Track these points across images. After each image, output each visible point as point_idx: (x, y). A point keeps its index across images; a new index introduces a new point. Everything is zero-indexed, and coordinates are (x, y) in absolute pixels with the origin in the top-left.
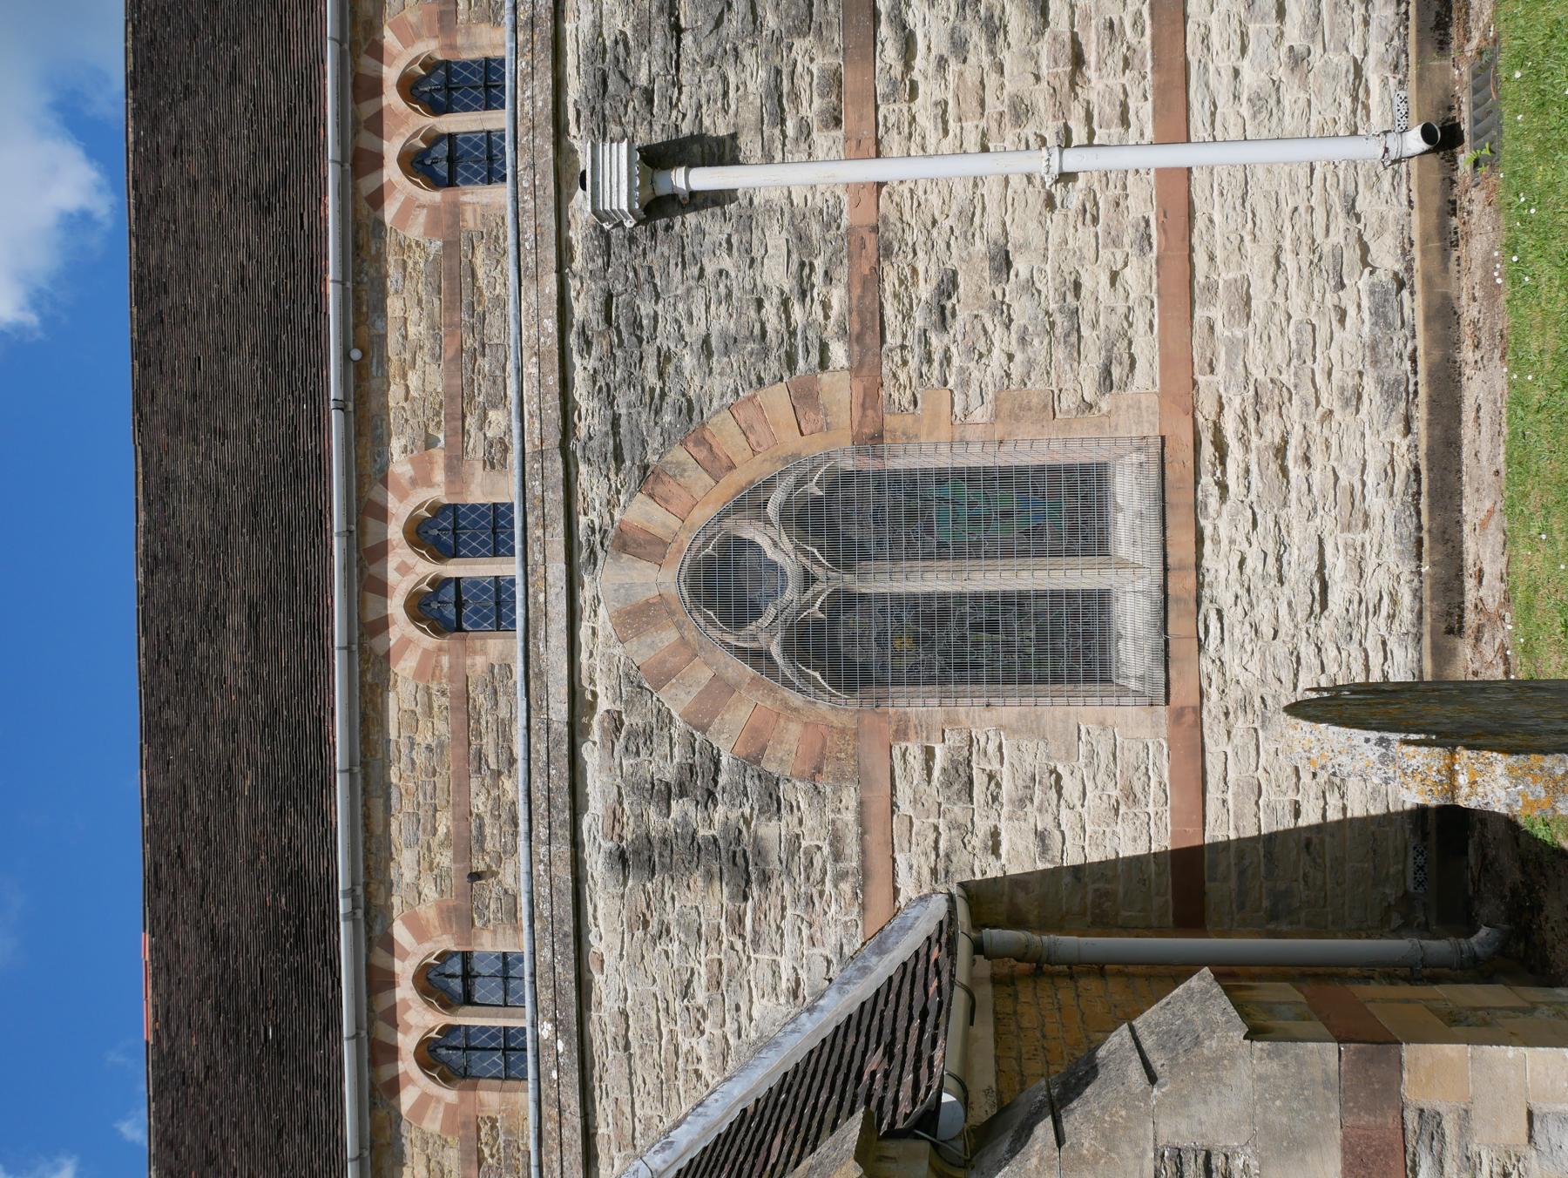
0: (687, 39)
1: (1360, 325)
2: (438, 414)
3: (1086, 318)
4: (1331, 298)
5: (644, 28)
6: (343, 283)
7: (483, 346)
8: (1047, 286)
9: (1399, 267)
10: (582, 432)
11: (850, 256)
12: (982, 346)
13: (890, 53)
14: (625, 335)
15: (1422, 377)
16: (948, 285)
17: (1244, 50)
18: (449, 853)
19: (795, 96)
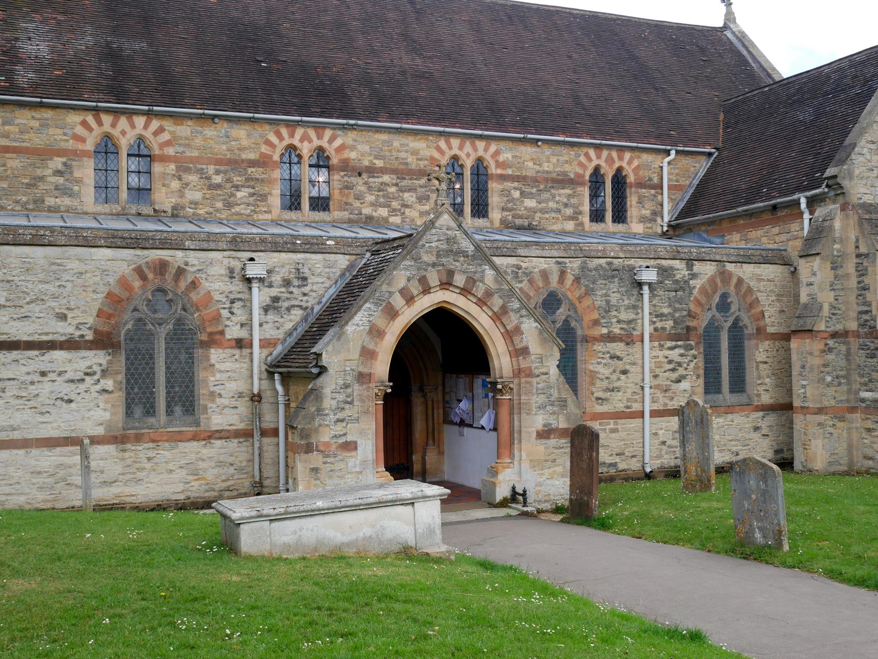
0: (674, 294)
3: (612, 393)
7: (541, 191)
13: (669, 344)
19: (661, 320)
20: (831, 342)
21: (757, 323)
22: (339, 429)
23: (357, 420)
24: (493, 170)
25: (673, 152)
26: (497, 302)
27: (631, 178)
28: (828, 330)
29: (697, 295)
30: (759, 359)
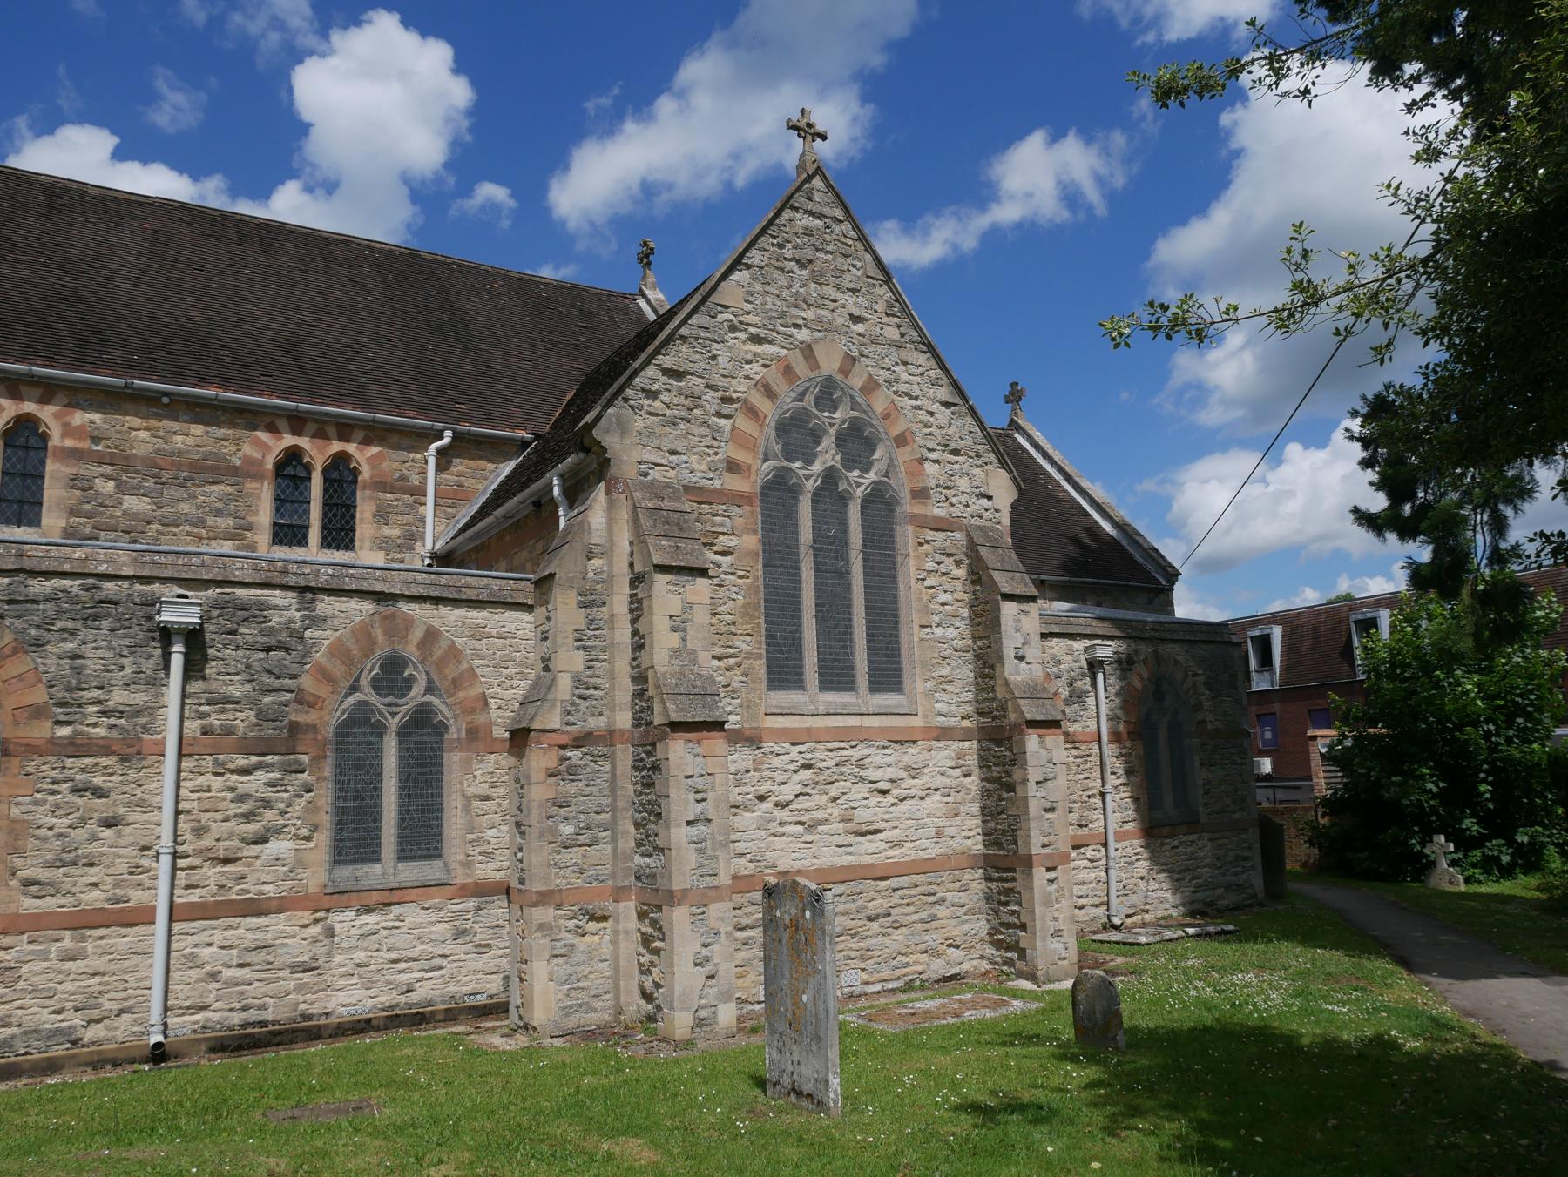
0: (262, 655)
1: (49, 1021)
2: (116, 448)
3: (72, 870)
4: (69, 1005)
5: (272, 632)
6: (216, 399)
8: (93, 848)
9: (86, 1040)
10: (30, 582)
11: (124, 739)
12: (59, 812)
13: (241, 762)
14: (90, 611)
15: (13, 1059)
16: (100, 793)
17: (223, 948)
19: (222, 711)
21: (469, 719)
25: (448, 433)
29: (323, 661)
30: (470, 791)
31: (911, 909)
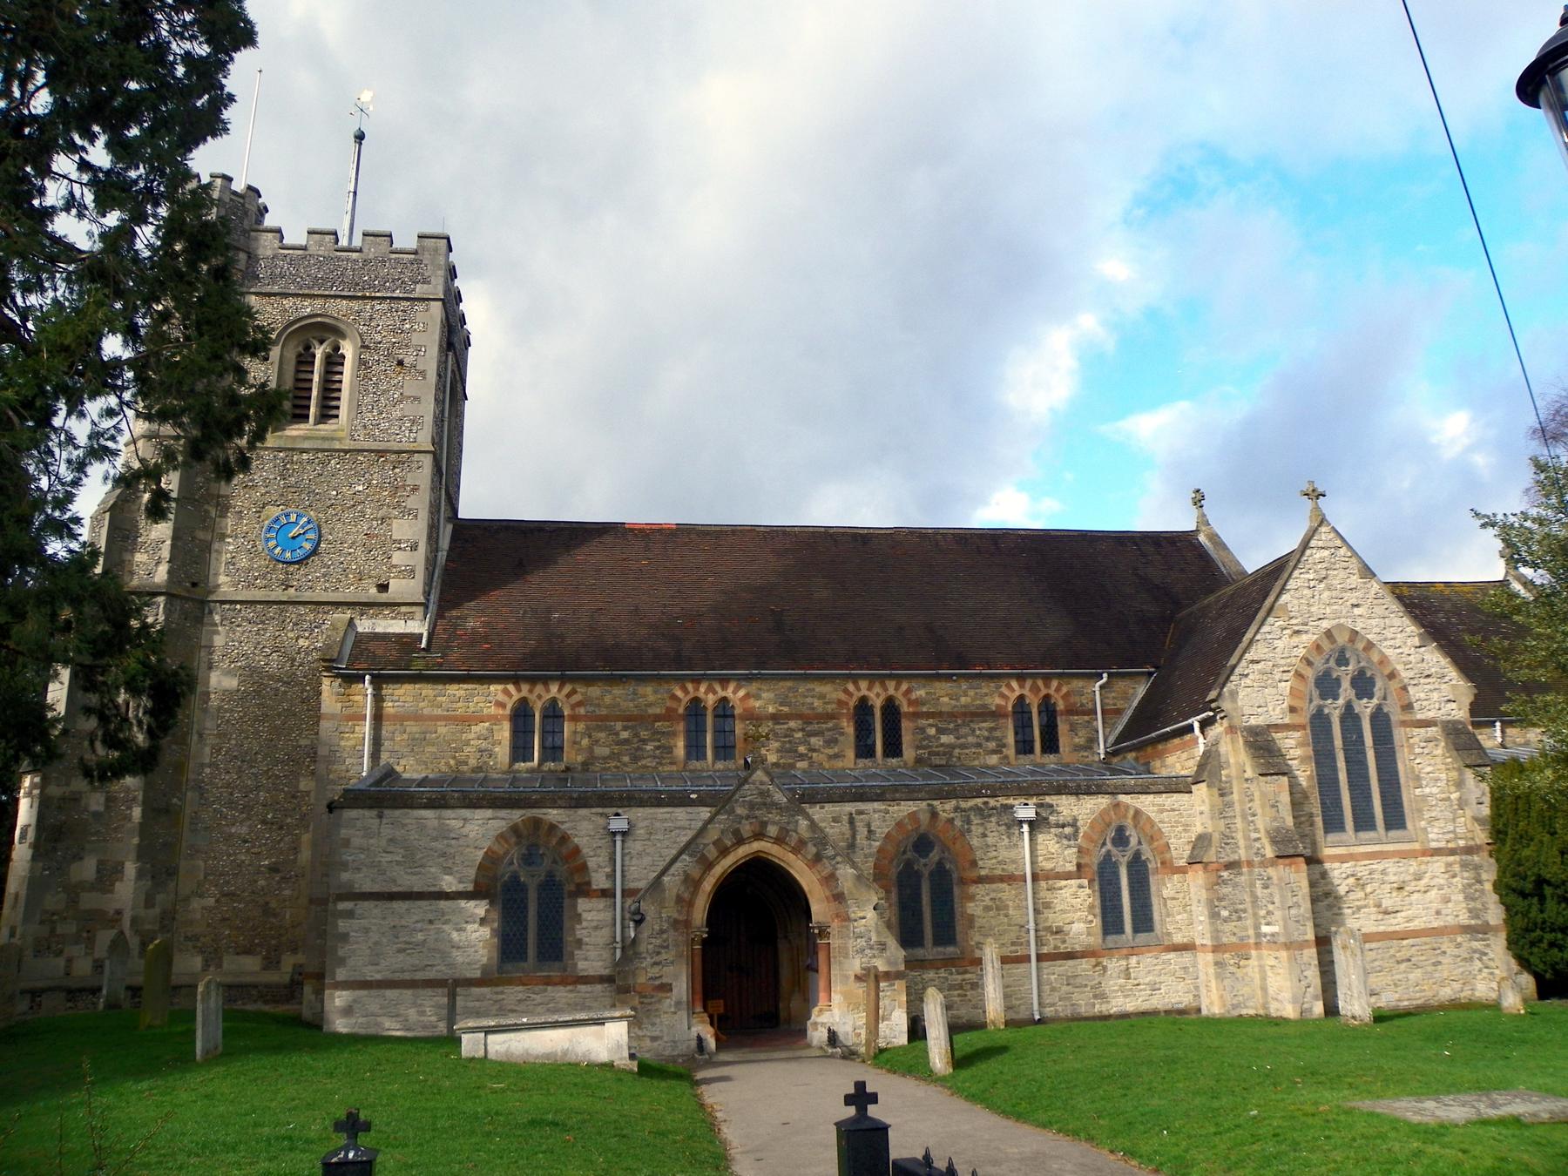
18: (774, 711)
20: (1225, 874)
22: (654, 971)
23: (672, 963)
24: (905, 708)
25: (1105, 675)
26: (812, 849)
27: (1061, 706)
28: (1221, 860)
31: (1424, 958)
